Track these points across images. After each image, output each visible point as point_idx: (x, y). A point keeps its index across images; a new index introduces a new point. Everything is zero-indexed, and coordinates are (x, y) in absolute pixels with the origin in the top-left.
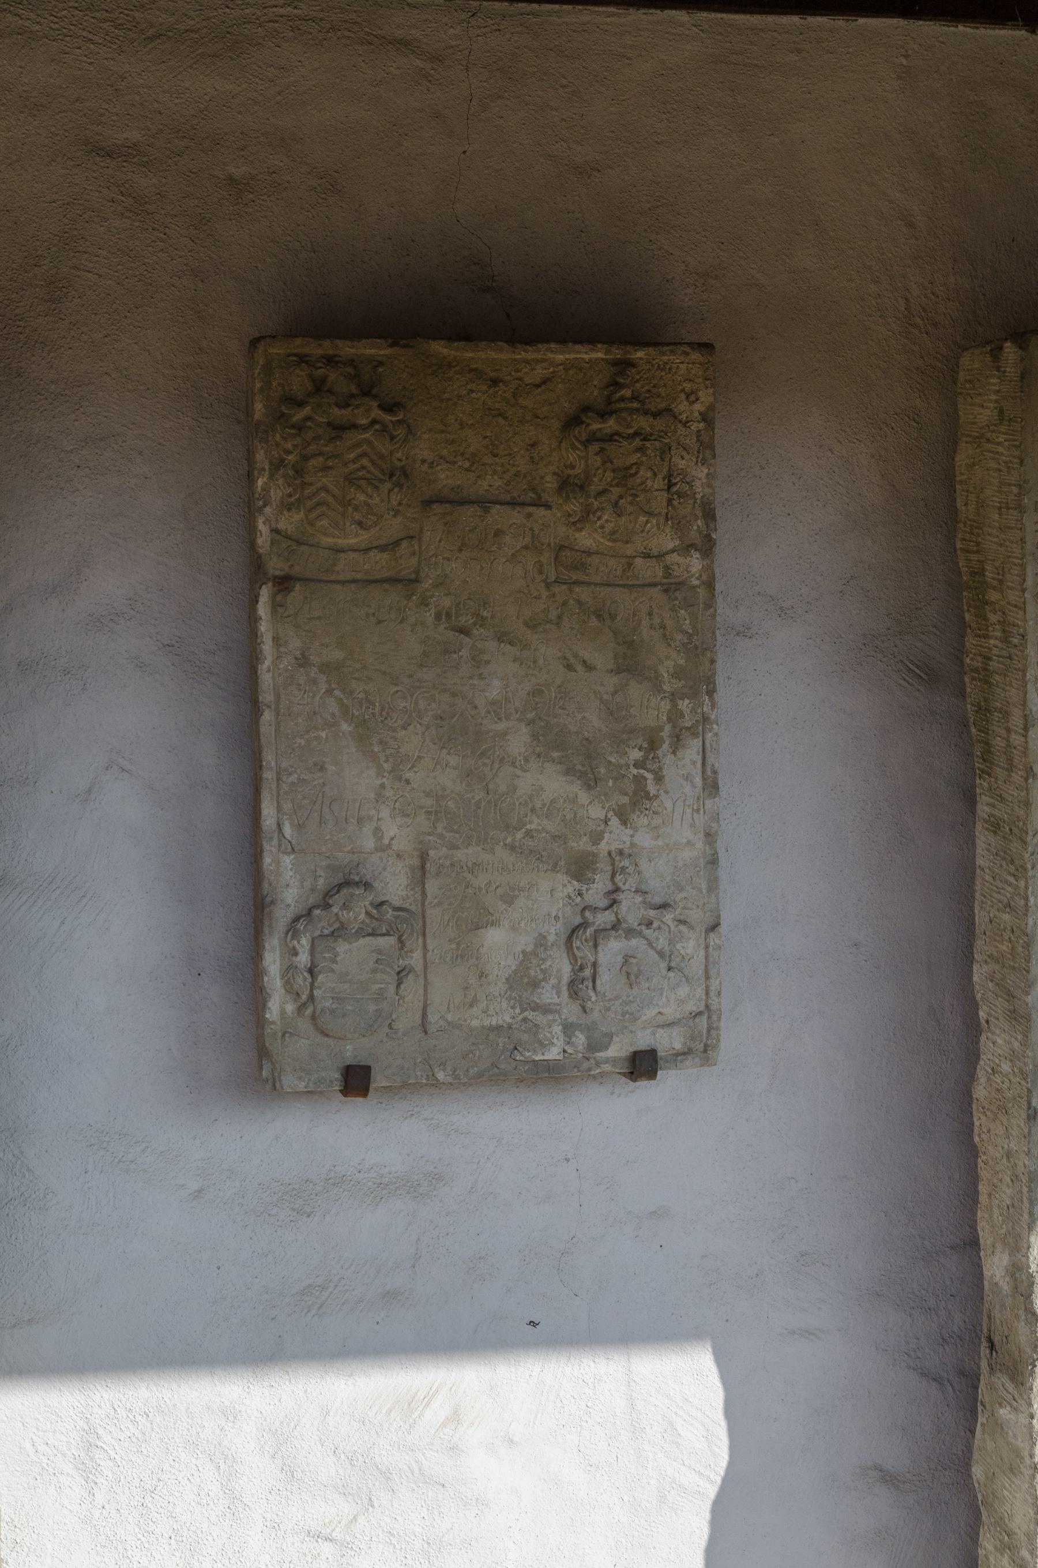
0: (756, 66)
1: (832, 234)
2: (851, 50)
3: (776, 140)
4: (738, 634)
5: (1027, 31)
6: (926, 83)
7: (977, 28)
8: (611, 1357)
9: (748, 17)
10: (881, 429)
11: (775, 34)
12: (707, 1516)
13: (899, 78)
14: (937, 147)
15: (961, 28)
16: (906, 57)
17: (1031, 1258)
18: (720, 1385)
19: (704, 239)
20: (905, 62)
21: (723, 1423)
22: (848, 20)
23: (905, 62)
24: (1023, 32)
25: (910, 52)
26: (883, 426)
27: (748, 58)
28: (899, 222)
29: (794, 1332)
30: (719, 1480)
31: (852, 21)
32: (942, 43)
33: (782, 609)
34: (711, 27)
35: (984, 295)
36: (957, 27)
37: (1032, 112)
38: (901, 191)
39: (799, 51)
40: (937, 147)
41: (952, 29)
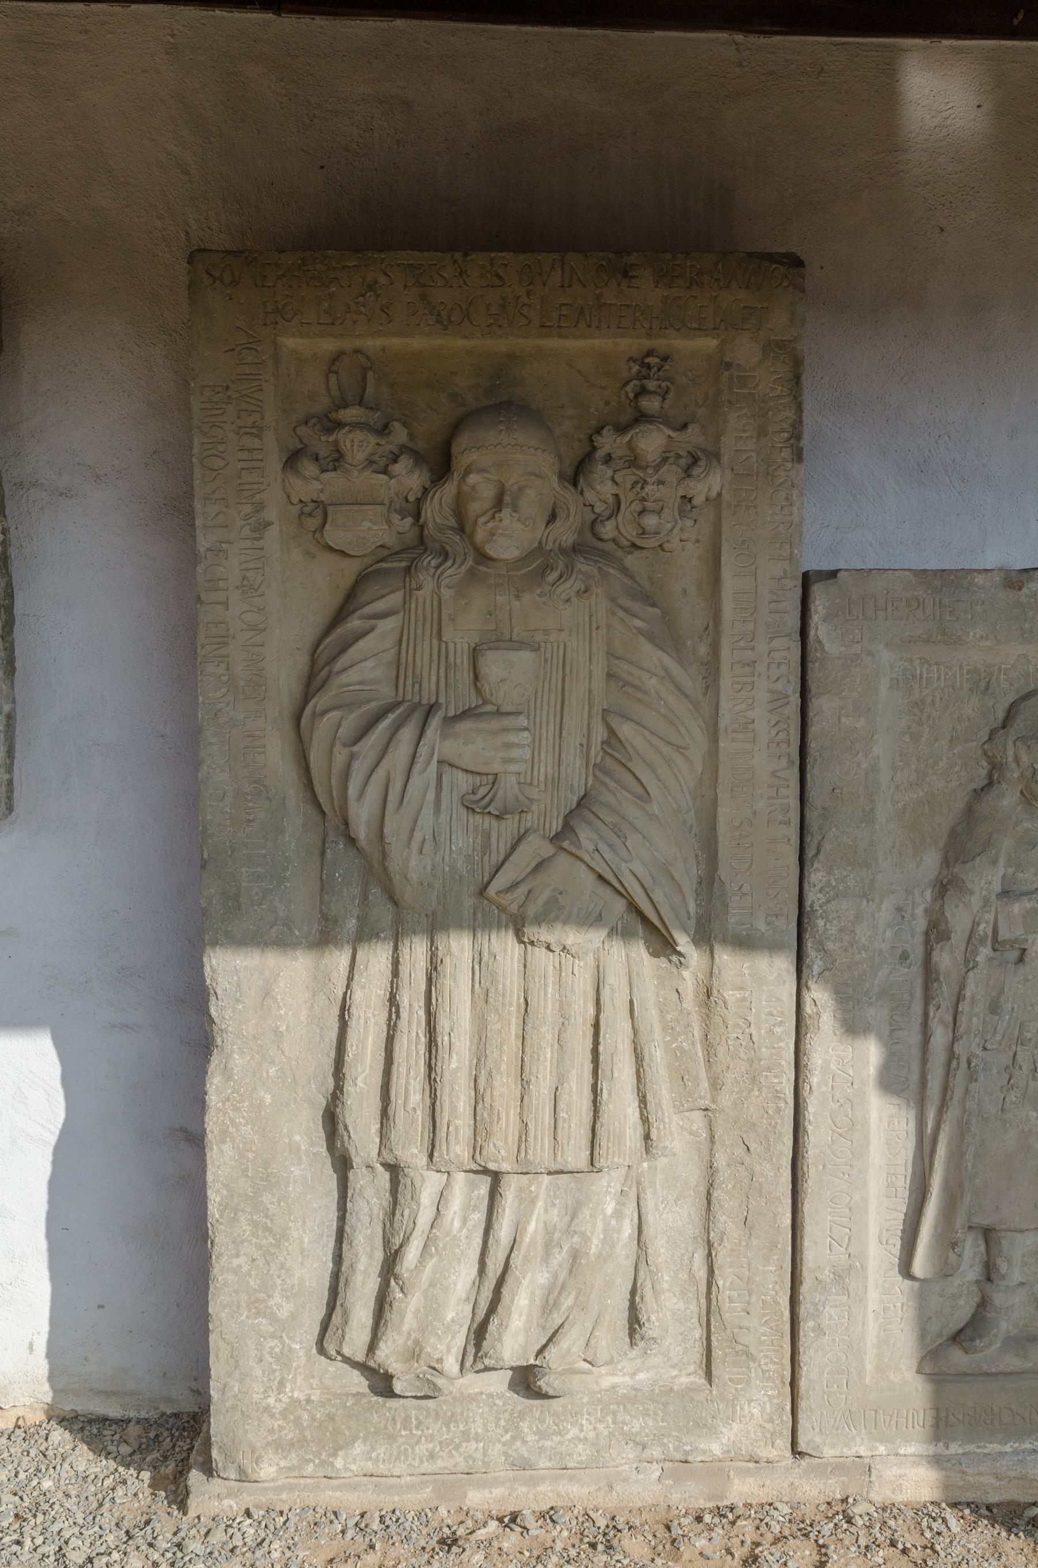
0: (53, 44)
1: (123, 180)
2: (127, 31)
3: (72, 104)
4: (61, 495)
5: (274, 14)
6: (191, 57)
7: (232, 12)
8: (1027, 1028)
9: (43, 4)
10: (171, 335)
11: (66, 18)
12: (50, 1158)
13: (167, 53)
14: (204, 109)
15: (218, 12)
16: (173, 36)
17: (206, 974)
18: (58, 1062)
19: (18, 184)
20: (171, 40)
21: (61, 1091)
22: (123, 7)
23: (171, 40)
24: (271, 15)
25: (176, 32)
26: (173, 333)
27: (46, 38)
28: (176, 170)
29: (114, 1026)
30: (57, 1132)
31: (127, 7)
32: (203, 24)
33: (97, 476)
34: (13, 13)
35: (251, 229)
36: (214, 11)
37: (282, 80)
38: (176, 145)
39: (86, 32)
40: (204, 109)
41: (211, 12)
